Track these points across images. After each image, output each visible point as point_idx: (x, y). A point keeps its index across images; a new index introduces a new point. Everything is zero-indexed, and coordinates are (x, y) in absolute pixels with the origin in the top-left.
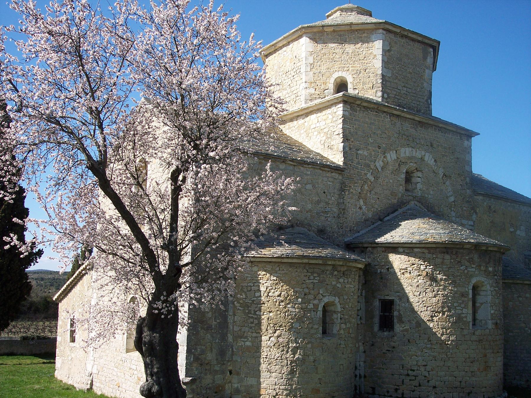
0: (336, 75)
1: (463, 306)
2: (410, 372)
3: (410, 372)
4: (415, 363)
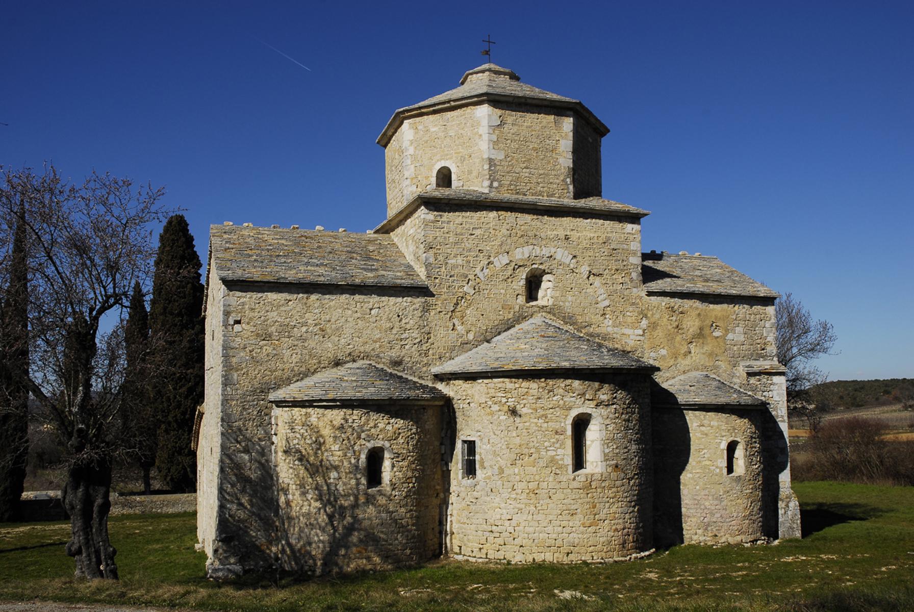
0: (438, 167)
1: (557, 445)
2: (494, 528)
3: (494, 528)
4: (498, 517)
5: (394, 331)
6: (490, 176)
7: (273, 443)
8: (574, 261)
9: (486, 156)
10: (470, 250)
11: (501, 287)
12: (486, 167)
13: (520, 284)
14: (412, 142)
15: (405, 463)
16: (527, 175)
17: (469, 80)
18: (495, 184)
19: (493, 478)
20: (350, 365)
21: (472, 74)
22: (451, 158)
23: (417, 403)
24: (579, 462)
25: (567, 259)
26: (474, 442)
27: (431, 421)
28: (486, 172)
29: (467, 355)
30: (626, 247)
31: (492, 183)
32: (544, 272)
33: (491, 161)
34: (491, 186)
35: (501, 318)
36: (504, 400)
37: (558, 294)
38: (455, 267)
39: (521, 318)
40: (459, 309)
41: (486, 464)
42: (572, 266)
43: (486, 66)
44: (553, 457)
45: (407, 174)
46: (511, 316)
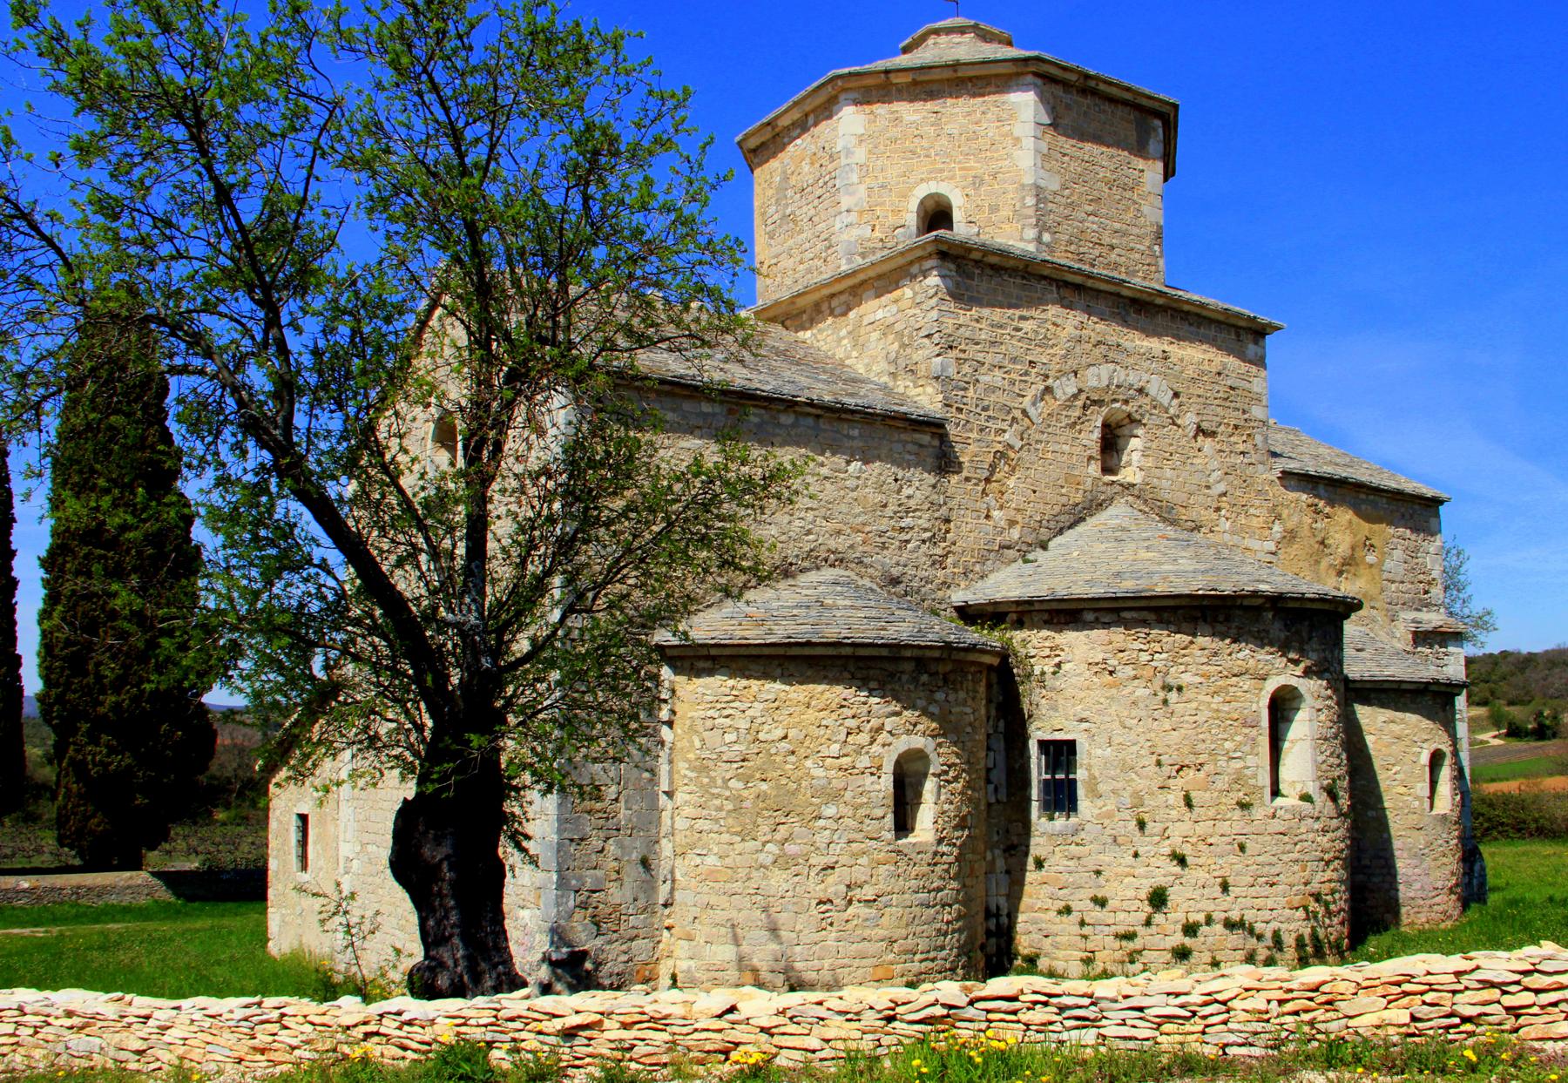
0: (921, 192)
5: (889, 512)
6: (1038, 220)
7: (662, 743)
8: (1175, 402)
9: (1029, 180)
10: (1014, 360)
11: (1063, 439)
12: (1030, 201)
13: (1092, 437)
14: (861, 140)
15: (959, 786)
16: (1095, 227)
17: (930, 41)
18: (1046, 237)
19: (1119, 816)
20: (813, 576)
21: (937, 32)
22: (951, 178)
23: (972, 657)
24: (903, 825)
25: (1165, 398)
26: (1071, 745)
27: (974, 707)
28: (1031, 212)
29: (1009, 569)
30: (1247, 385)
31: (1040, 233)
32: (1132, 420)
33: (1039, 192)
34: (1039, 240)
35: (1064, 500)
36: (1145, 657)
37: (1150, 463)
38: (991, 389)
39: (1094, 505)
40: (996, 476)
41: (1102, 788)
42: (1172, 411)
43: (948, 23)
44: (1238, 771)
45: (846, 201)
46: (1079, 498)
